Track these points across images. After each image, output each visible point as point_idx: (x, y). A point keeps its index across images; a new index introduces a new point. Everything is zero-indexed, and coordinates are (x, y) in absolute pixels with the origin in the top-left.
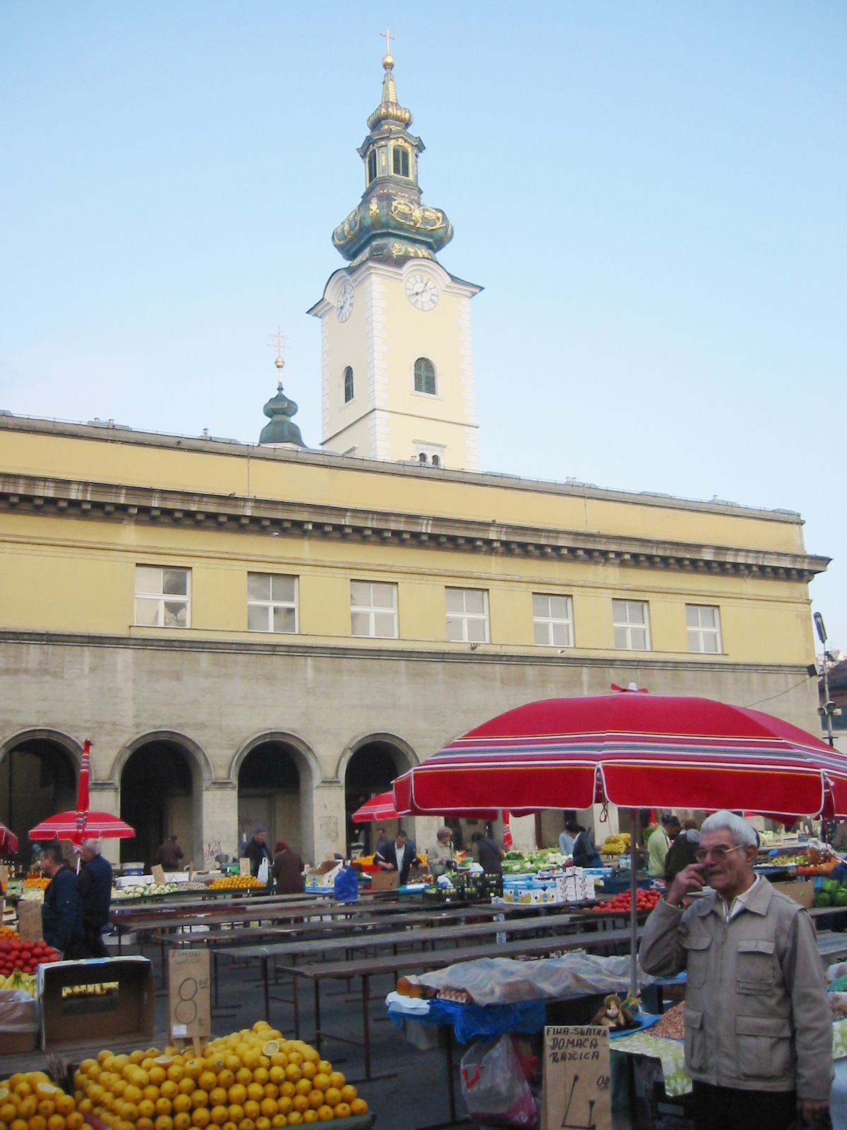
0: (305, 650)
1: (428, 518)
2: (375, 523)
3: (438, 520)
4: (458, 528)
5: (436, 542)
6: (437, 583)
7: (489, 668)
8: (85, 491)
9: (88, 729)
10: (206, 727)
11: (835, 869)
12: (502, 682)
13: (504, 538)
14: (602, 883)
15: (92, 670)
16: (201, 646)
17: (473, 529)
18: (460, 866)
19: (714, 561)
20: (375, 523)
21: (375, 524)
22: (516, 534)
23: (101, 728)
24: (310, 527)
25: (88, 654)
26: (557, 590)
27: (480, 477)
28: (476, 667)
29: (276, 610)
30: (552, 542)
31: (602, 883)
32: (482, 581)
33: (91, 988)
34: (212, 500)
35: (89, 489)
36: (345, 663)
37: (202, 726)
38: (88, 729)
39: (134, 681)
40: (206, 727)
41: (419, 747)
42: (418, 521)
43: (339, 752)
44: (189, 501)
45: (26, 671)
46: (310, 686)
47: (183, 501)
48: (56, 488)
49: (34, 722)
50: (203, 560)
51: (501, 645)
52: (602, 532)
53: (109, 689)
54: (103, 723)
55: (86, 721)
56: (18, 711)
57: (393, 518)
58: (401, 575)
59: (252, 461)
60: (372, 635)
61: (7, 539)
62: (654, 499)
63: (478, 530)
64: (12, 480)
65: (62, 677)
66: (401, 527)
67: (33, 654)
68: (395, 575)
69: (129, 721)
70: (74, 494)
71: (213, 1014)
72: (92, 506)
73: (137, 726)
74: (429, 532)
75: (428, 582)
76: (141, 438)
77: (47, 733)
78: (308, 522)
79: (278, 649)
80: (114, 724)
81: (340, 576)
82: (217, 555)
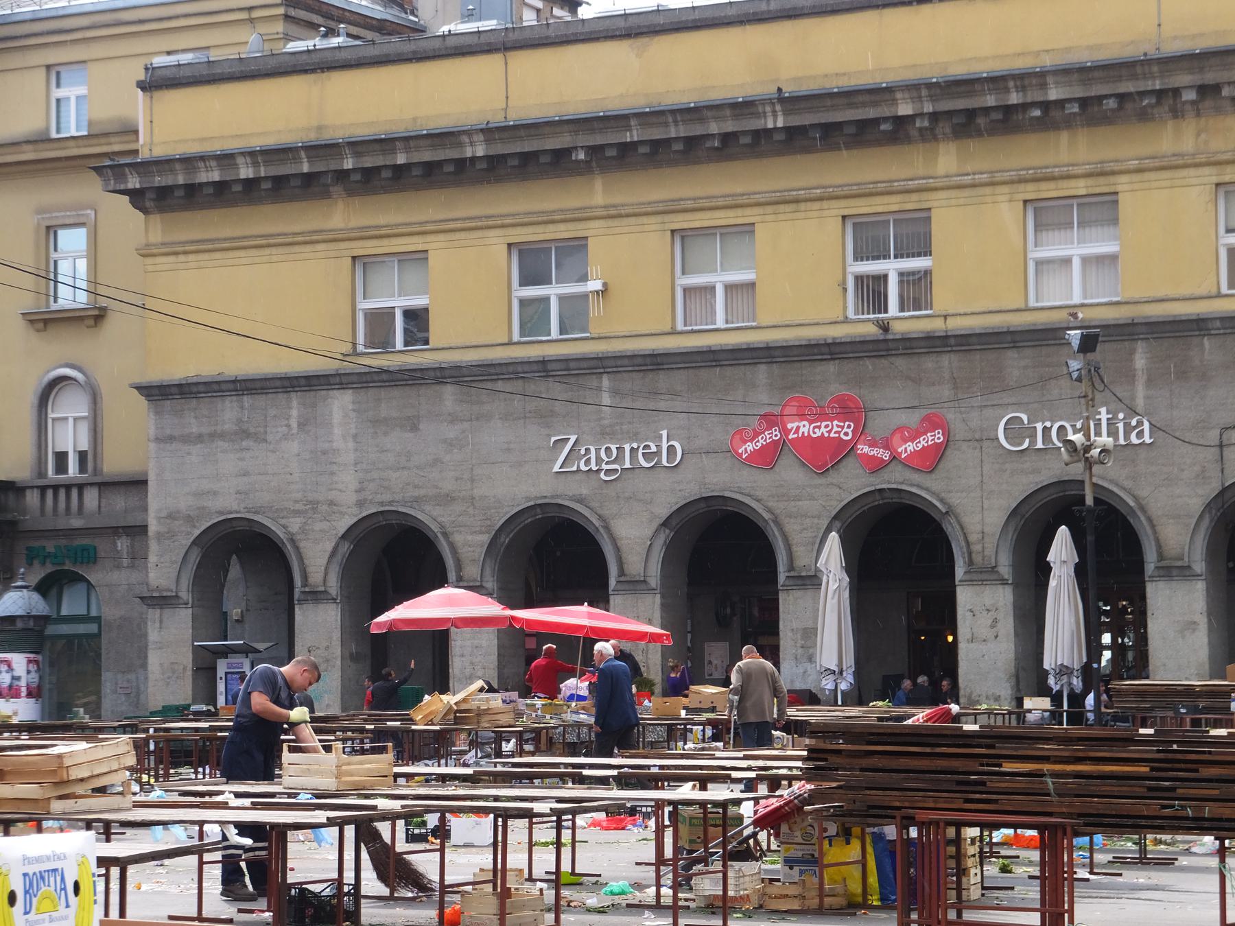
0: (592, 363)
2: (681, 128)
5: (796, 140)
7: (929, 363)
8: (255, 164)
9: (297, 513)
10: (453, 499)
12: (955, 388)
15: (301, 425)
16: (492, 371)
17: (864, 105)
18: (1106, 707)
20: (681, 128)
21: (683, 131)
23: (314, 510)
25: (295, 406)
27: (305, 57)
28: (901, 363)
30: (1033, 96)
32: (914, 197)
33: (247, 880)
35: (632, 123)
36: (663, 380)
37: (447, 499)
38: (297, 513)
39: (355, 436)
40: (453, 499)
41: (790, 517)
43: (649, 532)
44: (1119, 79)
45: (222, 436)
46: (606, 422)
48: (221, 167)
49: (235, 507)
50: (442, 237)
51: (945, 317)
52: (716, 96)
53: (324, 453)
54: (318, 503)
55: (297, 502)
56: (215, 493)
58: (757, 210)
60: (720, 323)
61: (508, 221)
65: (265, 441)
66: (730, 126)
67: (229, 411)
68: (748, 211)
69: (348, 497)
70: (246, 172)
72: (1198, 92)
73: (360, 504)
74: (682, 135)
75: (810, 214)
77: (246, 523)
79: (606, 363)
80: (332, 503)
81: (653, 227)
82: (459, 225)
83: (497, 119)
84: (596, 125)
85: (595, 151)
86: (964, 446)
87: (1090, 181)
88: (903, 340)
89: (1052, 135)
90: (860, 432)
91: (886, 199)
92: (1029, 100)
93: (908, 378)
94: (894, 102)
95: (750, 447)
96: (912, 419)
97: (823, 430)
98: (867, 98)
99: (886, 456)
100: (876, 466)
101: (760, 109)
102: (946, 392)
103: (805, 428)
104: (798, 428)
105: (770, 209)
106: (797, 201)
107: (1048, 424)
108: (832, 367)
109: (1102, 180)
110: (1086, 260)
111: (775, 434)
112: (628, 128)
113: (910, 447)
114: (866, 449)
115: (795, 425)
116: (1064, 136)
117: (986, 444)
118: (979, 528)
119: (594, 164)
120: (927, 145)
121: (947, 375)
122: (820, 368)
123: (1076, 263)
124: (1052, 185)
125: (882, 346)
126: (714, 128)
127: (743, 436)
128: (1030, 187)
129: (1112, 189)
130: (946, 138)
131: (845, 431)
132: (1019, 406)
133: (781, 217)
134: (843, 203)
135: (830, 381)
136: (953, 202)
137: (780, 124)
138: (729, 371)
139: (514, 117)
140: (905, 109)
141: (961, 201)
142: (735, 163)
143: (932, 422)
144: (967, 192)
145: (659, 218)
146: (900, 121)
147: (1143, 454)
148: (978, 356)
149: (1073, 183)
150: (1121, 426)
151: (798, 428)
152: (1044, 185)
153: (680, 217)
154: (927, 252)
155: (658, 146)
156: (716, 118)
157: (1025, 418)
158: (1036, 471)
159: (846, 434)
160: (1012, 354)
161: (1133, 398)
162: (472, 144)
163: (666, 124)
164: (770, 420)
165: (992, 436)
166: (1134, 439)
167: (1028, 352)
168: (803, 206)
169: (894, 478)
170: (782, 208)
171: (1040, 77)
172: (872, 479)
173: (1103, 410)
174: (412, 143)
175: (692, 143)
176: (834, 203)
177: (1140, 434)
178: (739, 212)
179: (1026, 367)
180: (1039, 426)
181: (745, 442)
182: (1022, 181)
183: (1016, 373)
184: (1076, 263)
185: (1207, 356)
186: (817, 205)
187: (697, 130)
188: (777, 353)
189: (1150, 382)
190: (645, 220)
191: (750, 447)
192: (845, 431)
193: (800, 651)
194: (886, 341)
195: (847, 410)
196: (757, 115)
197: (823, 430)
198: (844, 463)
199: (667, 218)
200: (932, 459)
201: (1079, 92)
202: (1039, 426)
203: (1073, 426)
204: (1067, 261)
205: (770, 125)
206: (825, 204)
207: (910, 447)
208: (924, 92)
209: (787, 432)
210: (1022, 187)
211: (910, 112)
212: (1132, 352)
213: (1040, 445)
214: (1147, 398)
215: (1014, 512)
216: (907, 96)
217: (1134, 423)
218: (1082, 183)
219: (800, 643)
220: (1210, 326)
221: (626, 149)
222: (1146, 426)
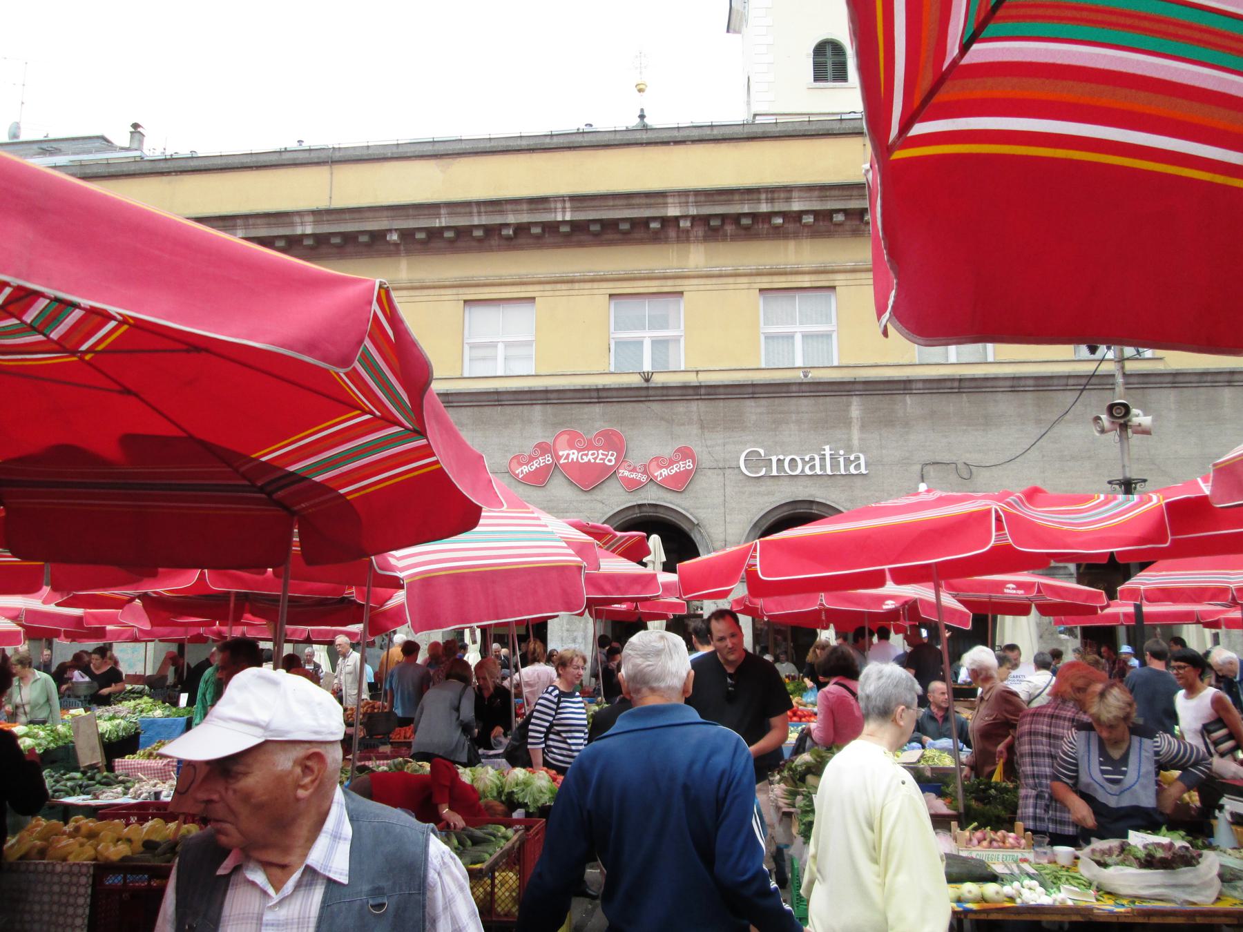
1: (562, 199)
3: (578, 200)
4: (614, 207)
6: (596, 292)
7: (680, 408)
11: (1088, 843)
12: (702, 427)
13: (693, 211)
14: (1217, 813)
17: (640, 206)
19: (682, 217)
21: (485, 220)
22: (714, 203)
24: (395, 237)
26: (806, 281)
28: (656, 407)
29: (806, 336)
30: (779, 207)
31: (1217, 813)
32: (670, 282)
34: (259, 221)
42: (546, 206)
44: (850, 197)
47: (531, 211)
51: (697, 372)
57: (509, 207)
59: (336, 168)
62: (162, 165)
63: (649, 206)
64: (855, 192)
66: (525, 218)
68: (530, 288)
71: (465, 760)
76: (665, 136)
78: (390, 230)
83: (323, 204)
84: (411, 212)
85: (407, 235)
86: (709, 473)
87: (813, 277)
88: (663, 388)
89: (781, 243)
90: (621, 459)
91: (647, 283)
92: (776, 209)
93: (662, 419)
94: (665, 205)
95: (526, 469)
96: (668, 451)
97: (590, 457)
98: (644, 201)
99: (644, 479)
100: (632, 486)
101: (552, 205)
102: (695, 430)
103: (574, 455)
104: (568, 455)
105: (548, 287)
106: (572, 281)
107: (781, 457)
108: (597, 409)
109: (822, 277)
110: (806, 336)
111: (548, 459)
112: (438, 216)
113: (665, 472)
114: (627, 473)
115: (566, 453)
116: (792, 245)
117: (728, 472)
118: (722, 537)
119: (402, 248)
120: (680, 246)
121: (695, 418)
122: (587, 409)
123: (798, 338)
124: (783, 278)
125: (644, 393)
126: (511, 219)
127: (518, 459)
128: (765, 279)
129: (831, 284)
130: (697, 240)
131: (610, 459)
132: (756, 443)
133: (558, 293)
134: (611, 285)
135: (596, 419)
136: (702, 288)
137: (568, 218)
138: (508, 410)
139: (338, 203)
140: (673, 211)
141: (709, 287)
142: (520, 252)
143: (686, 453)
144: (714, 281)
145: (454, 291)
146: (666, 221)
147: (858, 482)
148: (721, 403)
149: (799, 278)
150: (841, 460)
151: (568, 455)
152: (776, 278)
153: (472, 290)
154: (433, 455)
155: (463, 233)
156: (514, 211)
157: (762, 452)
158: (771, 493)
159: (610, 461)
160: (750, 403)
161: (849, 440)
162: (302, 224)
163: (471, 214)
164: (543, 449)
165: (734, 464)
166: (853, 471)
167: (763, 402)
168: (577, 286)
169: (652, 496)
170: (559, 286)
171: (787, 191)
172: (630, 497)
173: (827, 447)
174: (251, 221)
175: (490, 230)
176: (604, 285)
177: (858, 467)
178: (523, 288)
179: (761, 414)
180: (774, 459)
181: (522, 465)
182: (759, 274)
183: (754, 417)
184: (798, 338)
185: (909, 410)
186: (588, 285)
187: (497, 220)
188: (552, 396)
189: (863, 427)
190: (443, 291)
191: (526, 469)
192: (610, 459)
193: (565, 634)
194: (647, 388)
195: (612, 441)
196: (548, 210)
197: (590, 457)
198: (607, 483)
199: (461, 291)
200: (680, 483)
201: (817, 206)
202: (774, 459)
203: (802, 459)
204: (790, 337)
205: (559, 218)
206: (596, 285)
207: (665, 472)
208: (691, 199)
209: (559, 458)
210: (758, 279)
211: (678, 214)
212: (849, 405)
213: (774, 473)
214: (861, 439)
215: (755, 525)
216: (677, 200)
217: (852, 458)
218: (807, 278)
219: (566, 627)
220: (914, 386)
221: (434, 234)
222: (862, 461)
